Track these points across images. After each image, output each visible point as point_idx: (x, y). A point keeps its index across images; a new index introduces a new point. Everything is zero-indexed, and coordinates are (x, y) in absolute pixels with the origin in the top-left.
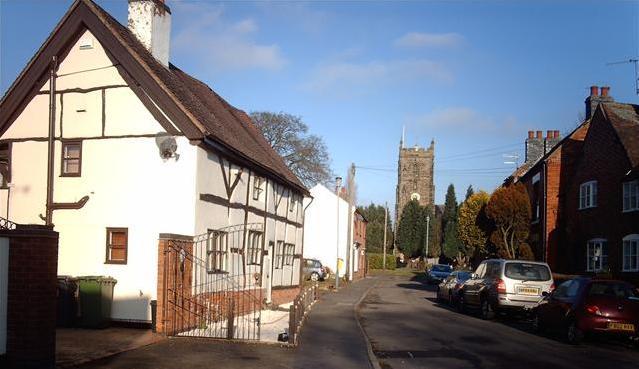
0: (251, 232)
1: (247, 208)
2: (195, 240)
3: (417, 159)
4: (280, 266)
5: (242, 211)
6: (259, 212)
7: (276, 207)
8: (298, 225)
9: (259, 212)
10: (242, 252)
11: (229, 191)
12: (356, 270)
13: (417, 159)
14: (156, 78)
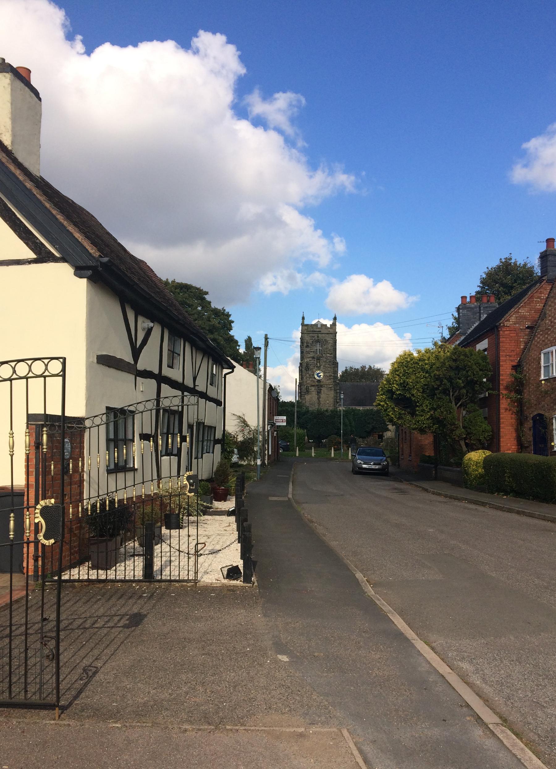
0: (165, 410)
1: (161, 379)
2: (88, 423)
3: (320, 335)
4: (200, 456)
5: (153, 382)
6: (174, 384)
7: (195, 379)
8: (218, 403)
9: (174, 384)
10: (179, 455)
11: (136, 353)
12: (270, 453)
13: (320, 335)
14: (71, 228)
